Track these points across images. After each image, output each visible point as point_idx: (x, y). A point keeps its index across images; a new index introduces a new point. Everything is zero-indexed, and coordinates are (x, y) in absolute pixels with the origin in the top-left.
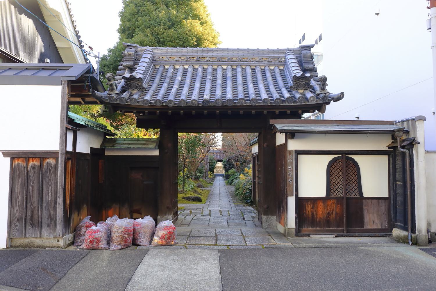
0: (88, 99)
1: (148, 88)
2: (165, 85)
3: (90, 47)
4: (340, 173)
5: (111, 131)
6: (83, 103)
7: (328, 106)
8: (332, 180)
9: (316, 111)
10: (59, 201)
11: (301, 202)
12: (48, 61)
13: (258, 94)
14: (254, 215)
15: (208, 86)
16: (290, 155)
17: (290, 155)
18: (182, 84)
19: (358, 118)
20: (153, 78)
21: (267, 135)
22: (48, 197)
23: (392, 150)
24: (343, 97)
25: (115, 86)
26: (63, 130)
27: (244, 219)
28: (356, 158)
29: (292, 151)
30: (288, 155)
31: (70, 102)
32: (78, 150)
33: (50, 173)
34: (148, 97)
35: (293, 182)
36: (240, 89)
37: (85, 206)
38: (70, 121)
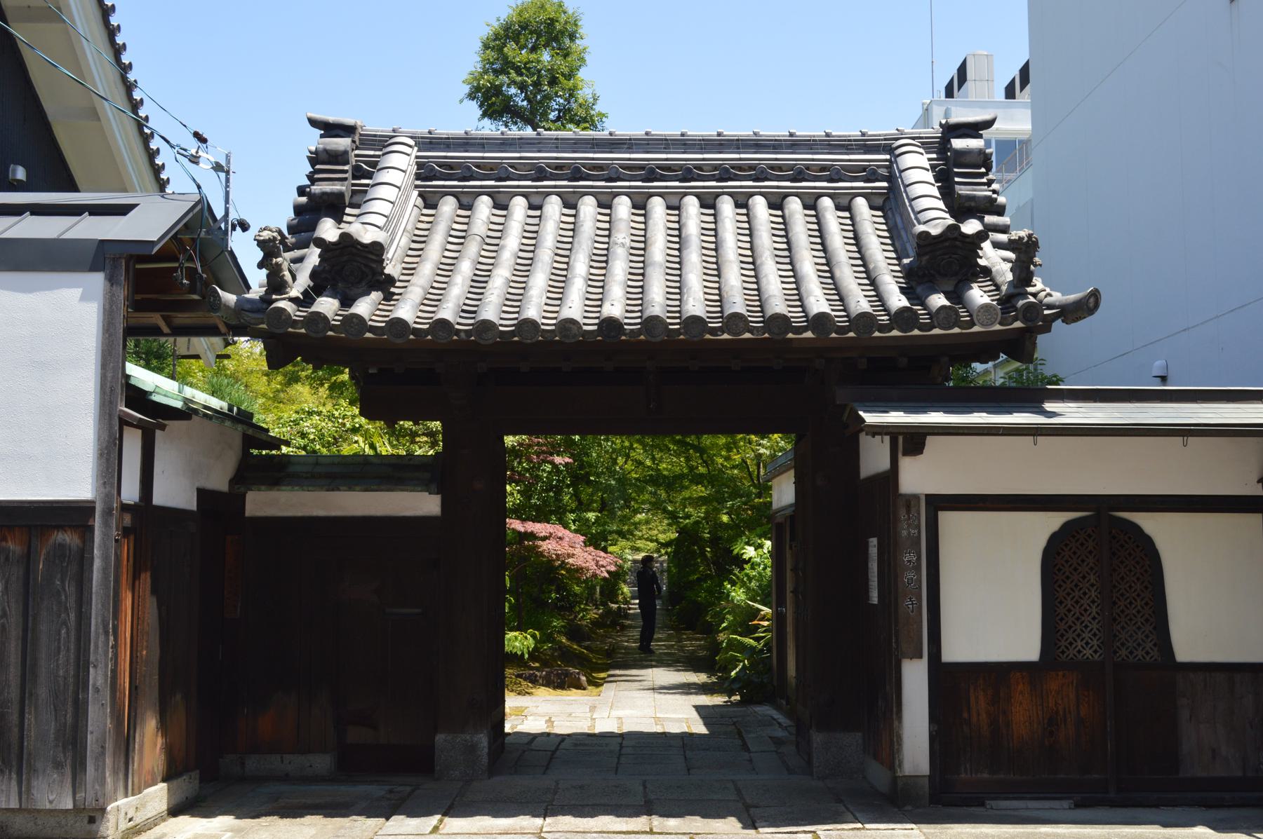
0: (182, 318)
1: (403, 278)
2: (465, 268)
3: (197, 135)
4: (1092, 578)
5: (267, 430)
6: (166, 330)
7: (1041, 339)
8: (1061, 603)
9: (1003, 357)
10: (95, 678)
11: (951, 682)
12: (21, 174)
13: (798, 295)
14: (780, 733)
15: (619, 268)
16: (908, 512)
17: (908, 512)
18: (525, 266)
20: (419, 242)
21: (827, 449)
22: (58, 666)
24: (1097, 305)
25: (287, 273)
26: (111, 427)
27: (745, 747)
28: (1149, 523)
29: (916, 497)
30: (902, 514)
31: (130, 331)
32: (159, 499)
33: (63, 582)
34: (406, 311)
35: (920, 607)
36: (734, 278)
37: (179, 697)
38: (138, 398)
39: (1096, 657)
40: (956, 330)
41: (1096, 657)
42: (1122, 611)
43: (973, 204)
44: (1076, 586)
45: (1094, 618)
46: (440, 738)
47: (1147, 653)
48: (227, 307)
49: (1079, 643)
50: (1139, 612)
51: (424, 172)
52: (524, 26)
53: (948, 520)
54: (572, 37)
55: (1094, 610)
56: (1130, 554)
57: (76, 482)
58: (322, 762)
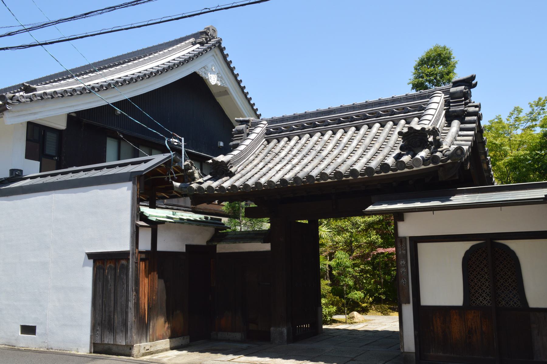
16: (401, 244)
17: (401, 244)
19: (29, 330)
23: (267, 247)
28: (512, 244)
29: (405, 238)
38: (143, 217)
39: (489, 304)
40: (406, 170)
41: (489, 304)
42: (502, 284)
43: (456, 114)
44: (479, 273)
45: (487, 287)
46: (272, 329)
47: (515, 303)
48: (176, 187)
49: (481, 298)
50: (510, 285)
51: (268, 132)
52: (429, 59)
53: (422, 247)
54: (449, 58)
55: (487, 284)
56: (505, 259)
57: (125, 245)
58: (238, 336)
